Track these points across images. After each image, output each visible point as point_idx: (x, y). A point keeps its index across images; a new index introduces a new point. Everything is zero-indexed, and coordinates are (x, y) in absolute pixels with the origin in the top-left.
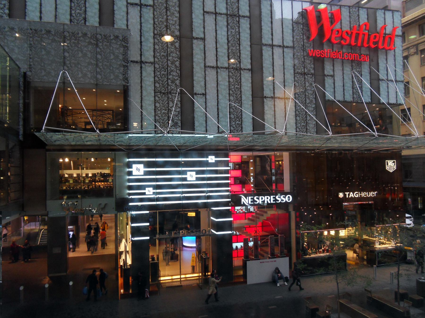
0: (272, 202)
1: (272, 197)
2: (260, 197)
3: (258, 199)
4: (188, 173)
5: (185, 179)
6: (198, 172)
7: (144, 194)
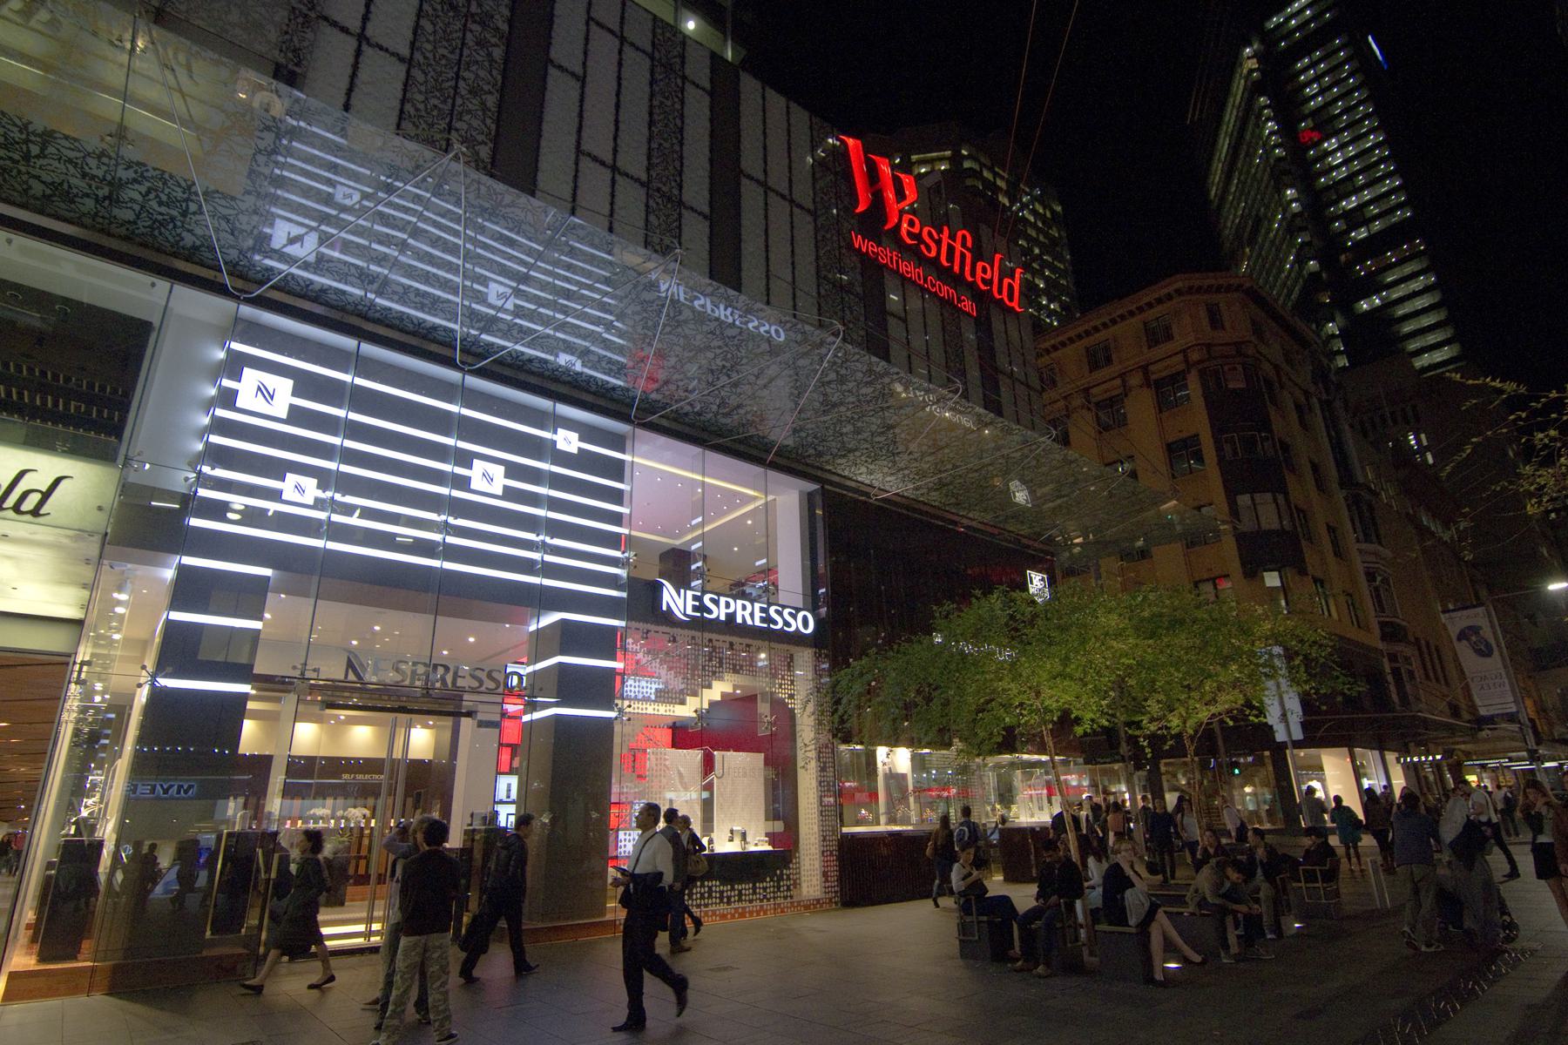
0: (757, 623)
1: (757, 606)
2: (723, 600)
3: (716, 602)
4: (476, 462)
5: (463, 483)
6: (513, 471)
7: (275, 495)
